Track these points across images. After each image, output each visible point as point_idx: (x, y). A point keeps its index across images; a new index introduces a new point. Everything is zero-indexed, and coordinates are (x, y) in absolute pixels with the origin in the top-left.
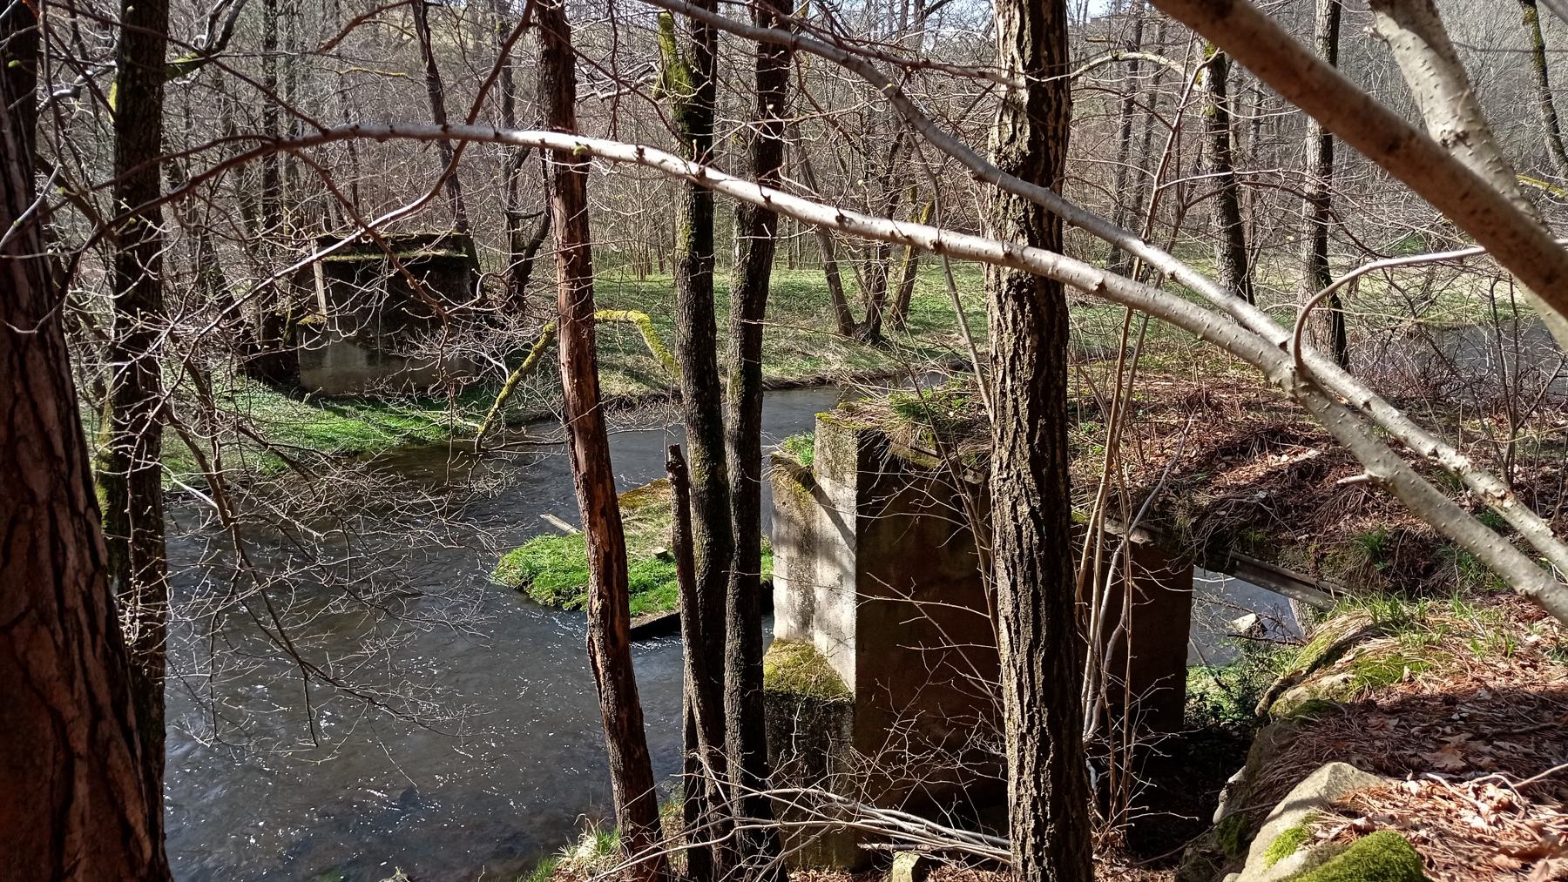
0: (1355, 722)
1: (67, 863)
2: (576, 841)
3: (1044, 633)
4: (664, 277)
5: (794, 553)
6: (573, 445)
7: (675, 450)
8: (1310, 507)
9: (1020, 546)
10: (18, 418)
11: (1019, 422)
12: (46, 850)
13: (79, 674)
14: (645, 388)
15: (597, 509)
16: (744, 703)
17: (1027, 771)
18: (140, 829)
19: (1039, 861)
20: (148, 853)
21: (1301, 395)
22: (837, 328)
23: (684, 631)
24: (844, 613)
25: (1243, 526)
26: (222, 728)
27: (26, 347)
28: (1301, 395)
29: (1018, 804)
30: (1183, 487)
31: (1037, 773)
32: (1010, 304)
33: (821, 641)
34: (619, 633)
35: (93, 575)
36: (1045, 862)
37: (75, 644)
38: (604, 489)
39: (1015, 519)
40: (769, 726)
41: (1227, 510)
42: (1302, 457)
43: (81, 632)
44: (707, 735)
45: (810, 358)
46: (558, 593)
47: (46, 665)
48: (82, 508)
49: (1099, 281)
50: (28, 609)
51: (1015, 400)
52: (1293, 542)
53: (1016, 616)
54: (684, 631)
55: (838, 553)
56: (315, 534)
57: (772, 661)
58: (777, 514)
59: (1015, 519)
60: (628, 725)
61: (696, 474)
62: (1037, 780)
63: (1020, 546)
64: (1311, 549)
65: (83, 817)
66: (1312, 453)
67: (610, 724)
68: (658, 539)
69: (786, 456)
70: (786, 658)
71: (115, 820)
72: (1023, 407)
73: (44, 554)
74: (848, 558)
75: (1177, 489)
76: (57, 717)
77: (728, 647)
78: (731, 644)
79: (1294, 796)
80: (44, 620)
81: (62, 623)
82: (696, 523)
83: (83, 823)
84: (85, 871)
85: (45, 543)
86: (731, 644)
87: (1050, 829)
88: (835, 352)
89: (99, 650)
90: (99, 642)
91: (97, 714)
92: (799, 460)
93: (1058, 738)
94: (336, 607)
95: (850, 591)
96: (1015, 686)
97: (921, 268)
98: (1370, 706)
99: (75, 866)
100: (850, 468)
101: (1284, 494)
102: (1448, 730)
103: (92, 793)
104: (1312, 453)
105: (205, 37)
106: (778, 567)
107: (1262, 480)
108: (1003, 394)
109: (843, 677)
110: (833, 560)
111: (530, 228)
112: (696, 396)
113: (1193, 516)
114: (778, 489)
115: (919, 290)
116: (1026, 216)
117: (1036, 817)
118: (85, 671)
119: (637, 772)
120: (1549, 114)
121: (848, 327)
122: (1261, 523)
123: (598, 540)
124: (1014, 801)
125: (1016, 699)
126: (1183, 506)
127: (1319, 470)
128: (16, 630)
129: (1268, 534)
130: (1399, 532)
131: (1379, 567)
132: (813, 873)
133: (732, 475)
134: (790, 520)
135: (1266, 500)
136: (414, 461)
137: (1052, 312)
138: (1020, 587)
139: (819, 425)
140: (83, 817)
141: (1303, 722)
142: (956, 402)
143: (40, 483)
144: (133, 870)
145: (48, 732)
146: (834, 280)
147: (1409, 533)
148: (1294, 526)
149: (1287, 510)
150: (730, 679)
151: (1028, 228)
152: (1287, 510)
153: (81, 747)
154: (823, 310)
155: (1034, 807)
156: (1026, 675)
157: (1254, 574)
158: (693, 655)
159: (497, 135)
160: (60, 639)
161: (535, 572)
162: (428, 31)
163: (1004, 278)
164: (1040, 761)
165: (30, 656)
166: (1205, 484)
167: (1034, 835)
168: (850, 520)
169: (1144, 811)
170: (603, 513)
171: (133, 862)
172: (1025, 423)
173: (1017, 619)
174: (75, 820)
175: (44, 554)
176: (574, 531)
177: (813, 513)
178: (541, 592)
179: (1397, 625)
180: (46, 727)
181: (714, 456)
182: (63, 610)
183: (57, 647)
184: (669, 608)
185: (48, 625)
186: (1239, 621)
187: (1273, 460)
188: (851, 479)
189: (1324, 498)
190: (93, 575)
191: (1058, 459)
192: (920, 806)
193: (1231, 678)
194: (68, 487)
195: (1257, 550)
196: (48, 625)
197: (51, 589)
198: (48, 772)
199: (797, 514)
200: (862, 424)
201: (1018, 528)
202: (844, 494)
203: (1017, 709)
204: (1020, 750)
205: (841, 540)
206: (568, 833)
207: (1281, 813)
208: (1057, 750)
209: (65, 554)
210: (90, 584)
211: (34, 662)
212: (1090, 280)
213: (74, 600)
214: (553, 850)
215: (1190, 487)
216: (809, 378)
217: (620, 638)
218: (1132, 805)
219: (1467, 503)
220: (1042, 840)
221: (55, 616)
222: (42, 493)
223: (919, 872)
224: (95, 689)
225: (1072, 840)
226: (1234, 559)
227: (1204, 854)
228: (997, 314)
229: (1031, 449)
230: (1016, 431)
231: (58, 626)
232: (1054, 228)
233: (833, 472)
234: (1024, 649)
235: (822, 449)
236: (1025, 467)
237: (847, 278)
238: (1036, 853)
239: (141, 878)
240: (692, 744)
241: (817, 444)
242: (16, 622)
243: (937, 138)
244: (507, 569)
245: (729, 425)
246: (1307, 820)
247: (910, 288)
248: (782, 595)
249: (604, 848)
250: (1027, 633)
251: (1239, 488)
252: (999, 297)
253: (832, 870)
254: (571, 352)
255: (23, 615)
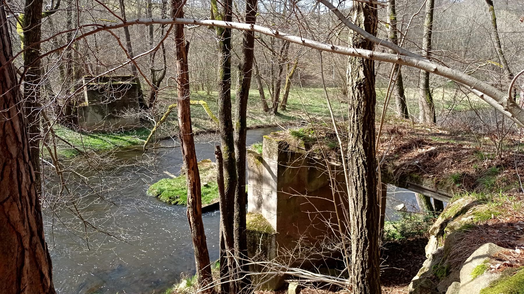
0: (484, 231)
1: (22, 287)
2: (179, 282)
3: (367, 204)
4: (204, 92)
5: (255, 183)
6: (182, 145)
7: (218, 147)
8: (434, 166)
9: (359, 174)
10: (7, 127)
11: (359, 131)
12: (15, 283)
13: (26, 220)
14: (198, 129)
15: (191, 167)
16: (240, 234)
17: (359, 252)
18: (47, 275)
19: (363, 283)
20: (49, 284)
21: (510, 108)
22: (263, 109)
23: (220, 209)
24: (273, 201)
25: (411, 172)
26: (67, 242)
27: (10, 102)
28: (510, 108)
29: (356, 263)
30: (390, 160)
31: (363, 252)
32: (357, 90)
33: (264, 212)
34: (198, 210)
35: (31, 185)
36: (365, 283)
37: (25, 209)
38: (193, 161)
39: (357, 165)
40: (247, 241)
41: (405, 167)
42: (429, 150)
43: (27, 205)
44: (228, 245)
45: (254, 120)
46: (170, 198)
47: (15, 216)
48: (27, 161)
49: (435, 68)
50: (9, 196)
51: (358, 124)
52: (428, 177)
53: (357, 198)
54: (220, 209)
55: (271, 183)
56: (85, 178)
57: (249, 219)
58: (249, 170)
59: (357, 165)
60: (201, 241)
61: (225, 157)
62: (363, 254)
63: (359, 174)
64: (434, 180)
65: (27, 271)
66: (432, 148)
67: (195, 241)
68: (204, 180)
69: (253, 150)
70: (252, 218)
71: (38, 272)
72: (361, 126)
73: (15, 177)
74: (274, 184)
75: (388, 160)
76: (19, 235)
77: (235, 214)
78: (236, 213)
79: (474, 254)
80: (15, 200)
81: (21, 201)
82: (225, 172)
83: (27, 273)
84: (28, 290)
85: (15, 172)
86: (236, 213)
87: (367, 271)
88: (262, 117)
89: (33, 211)
90: (33, 209)
91: (32, 234)
92: (257, 151)
93: (371, 240)
94: (96, 202)
95: (275, 195)
96: (356, 222)
97: (291, 90)
98: (486, 225)
99: (25, 289)
100: (275, 154)
101: (424, 162)
102: (518, 233)
103: (31, 262)
104: (432, 148)
105: (50, 6)
106: (250, 187)
107: (417, 157)
108: (354, 122)
109: (272, 225)
110: (269, 185)
111: (159, 75)
112: (224, 129)
113: (394, 169)
114: (250, 161)
115: (290, 97)
116: (363, 60)
117: (362, 267)
118: (28, 219)
119: (204, 258)
120: (498, 41)
121: (267, 109)
122: (417, 171)
123: (191, 178)
124: (354, 262)
125: (356, 227)
126: (390, 166)
127: (436, 154)
128: (5, 204)
129: (420, 175)
130: (464, 174)
131: (458, 185)
132: (262, 291)
133: (236, 156)
134: (254, 172)
135: (419, 164)
136: (122, 153)
137: (371, 94)
138: (358, 188)
139: (264, 139)
140: (27, 271)
141: (465, 232)
142: (311, 132)
143: (14, 150)
144: (44, 290)
145: (16, 240)
146: (262, 93)
147: (467, 174)
148: (428, 172)
149: (426, 167)
150: (236, 225)
151: (363, 64)
152: (426, 167)
153: (27, 246)
154: (258, 103)
155: (362, 264)
156: (360, 219)
157: (414, 188)
158: (224, 217)
159: (195, 21)
160: (20, 207)
161: (162, 191)
162: (124, 7)
163: (354, 82)
164: (364, 248)
165: (10, 213)
166: (397, 158)
167: (362, 274)
168: (275, 171)
169: (387, 267)
170: (193, 169)
171: (44, 287)
172: (361, 132)
173: (357, 199)
174: (25, 272)
175: (15, 177)
176: (175, 177)
177: (262, 169)
178: (164, 198)
179: (485, 201)
180: (15, 238)
181: (231, 149)
182: (21, 197)
183: (19, 210)
184: (209, 203)
185: (16, 202)
186: (399, 206)
187: (420, 151)
188: (276, 157)
189: (438, 163)
190: (31, 185)
191: (372, 144)
192: (307, 266)
193: (398, 225)
194: (23, 153)
195: (416, 181)
196: (16, 202)
197: (17, 189)
198: (16, 255)
199: (256, 170)
200: (279, 139)
201: (358, 168)
202: (273, 163)
203: (357, 230)
204: (357, 244)
205: (272, 178)
206: (176, 279)
207: (471, 261)
208: (371, 244)
209: (22, 177)
210: (30, 188)
211: (11, 215)
212: (431, 68)
213: (25, 193)
214: (171, 286)
215: (393, 159)
216: (254, 126)
217: (199, 212)
218: (382, 265)
219: (486, 164)
220: (364, 275)
221: (19, 199)
222: (14, 155)
223: (298, 291)
224: (31, 225)
225: (374, 275)
226: (408, 183)
227: (428, 278)
228: (352, 94)
229: (363, 141)
230: (358, 134)
231: (19, 202)
232: (372, 65)
233: (269, 155)
234: (359, 210)
235: (265, 148)
236: (361, 147)
237: (266, 93)
238: (362, 280)
239: (47, 293)
240: (223, 247)
241: (264, 146)
242: (5, 201)
243: (350, 25)
244: (152, 190)
245: (235, 139)
246: (485, 262)
247: (287, 96)
248: (251, 197)
249: (189, 284)
250: (360, 204)
251: (409, 160)
252: (353, 88)
253: (268, 290)
254: (182, 113)
255: (8, 198)
